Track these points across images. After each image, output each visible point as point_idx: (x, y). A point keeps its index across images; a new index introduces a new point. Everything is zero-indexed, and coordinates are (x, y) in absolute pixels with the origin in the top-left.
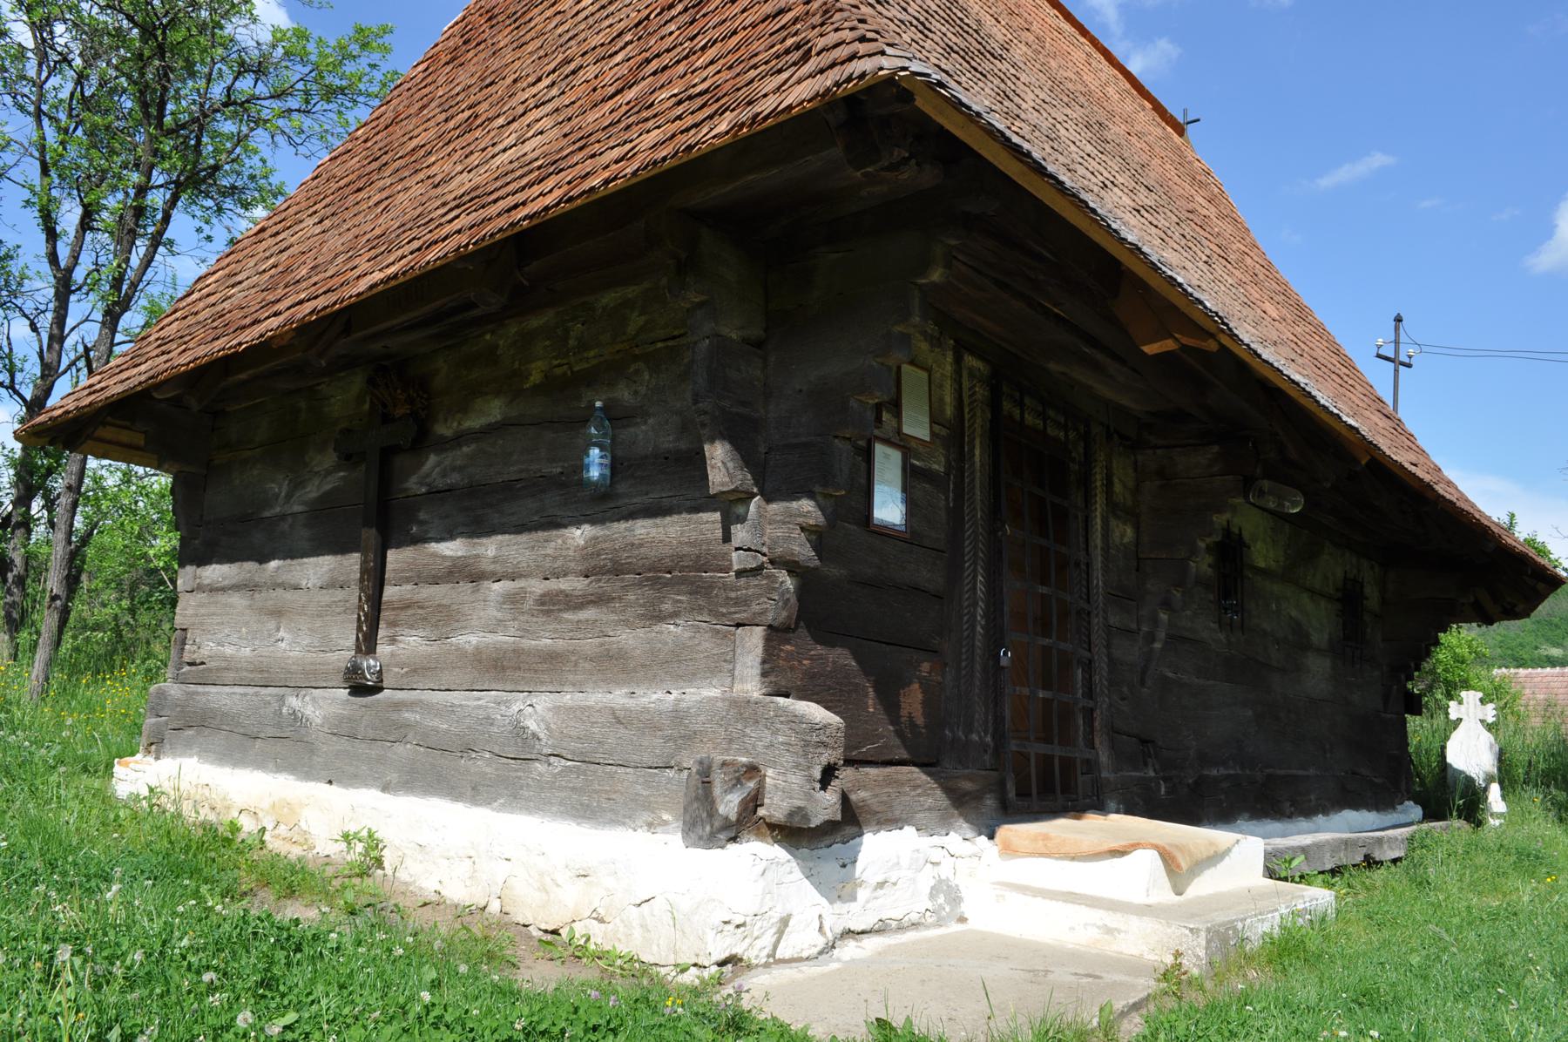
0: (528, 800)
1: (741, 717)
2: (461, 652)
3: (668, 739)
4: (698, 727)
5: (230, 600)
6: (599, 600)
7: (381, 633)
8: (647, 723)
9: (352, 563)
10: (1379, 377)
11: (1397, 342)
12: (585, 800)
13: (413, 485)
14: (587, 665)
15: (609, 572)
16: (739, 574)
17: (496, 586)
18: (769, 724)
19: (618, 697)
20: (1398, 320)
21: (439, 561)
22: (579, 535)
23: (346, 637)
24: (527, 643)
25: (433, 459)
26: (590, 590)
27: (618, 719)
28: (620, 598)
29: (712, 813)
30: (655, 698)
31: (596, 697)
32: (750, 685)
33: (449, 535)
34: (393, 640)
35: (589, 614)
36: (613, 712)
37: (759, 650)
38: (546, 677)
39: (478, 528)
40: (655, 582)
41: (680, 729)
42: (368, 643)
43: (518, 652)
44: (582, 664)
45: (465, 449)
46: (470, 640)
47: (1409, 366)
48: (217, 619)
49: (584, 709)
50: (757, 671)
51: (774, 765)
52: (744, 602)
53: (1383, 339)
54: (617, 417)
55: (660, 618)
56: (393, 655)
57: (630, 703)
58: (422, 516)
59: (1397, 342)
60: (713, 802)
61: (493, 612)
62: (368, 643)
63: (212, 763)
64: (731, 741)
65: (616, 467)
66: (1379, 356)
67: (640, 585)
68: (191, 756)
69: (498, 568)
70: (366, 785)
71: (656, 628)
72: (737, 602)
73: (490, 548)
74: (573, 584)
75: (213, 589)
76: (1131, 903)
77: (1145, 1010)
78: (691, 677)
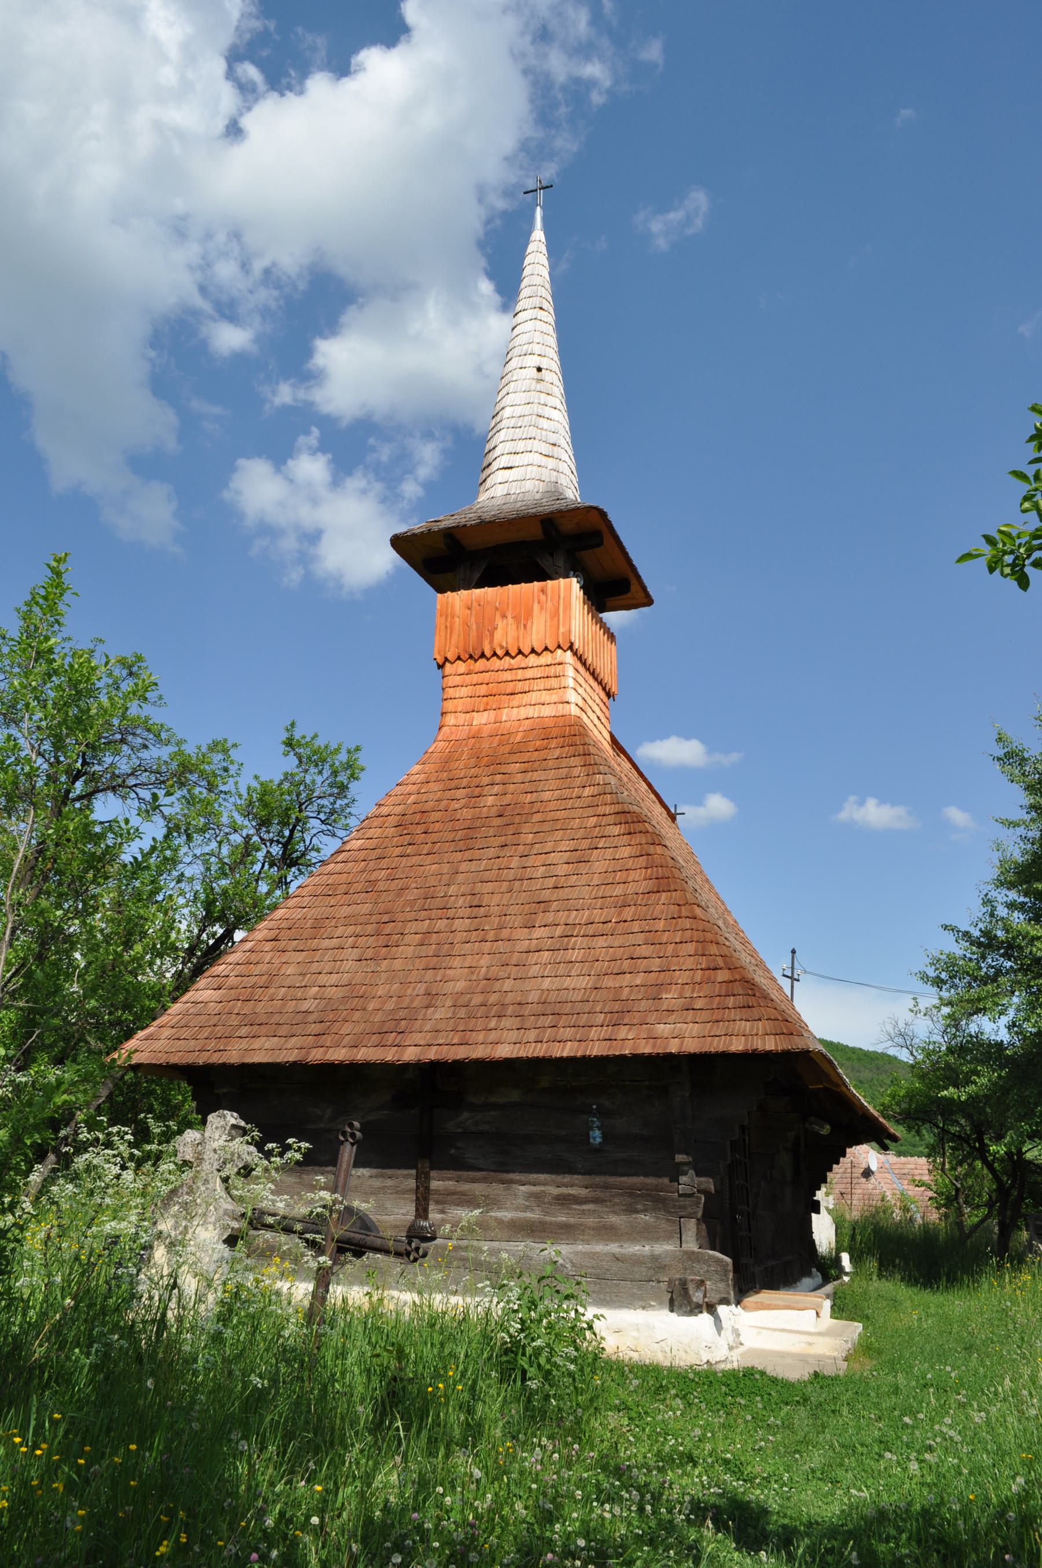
1: (689, 1259)
3: (649, 1268)
4: (667, 1263)
6: (596, 1201)
7: (431, 1207)
8: (637, 1261)
10: (785, 984)
11: (793, 968)
12: (602, 1297)
14: (591, 1232)
15: (601, 1187)
16: (680, 1195)
17: (522, 1188)
18: (706, 1262)
19: (614, 1248)
20: (793, 952)
24: (548, 1219)
25: (465, 1115)
26: (590, 1195)
27: (617, 1258)
28: (610, 1201)
29: (690, 1302)
30: (635, 1249)
31: (599, 1248)
32: (691, 1245)
36: (614, 1255)
37: (695, 1229)
40: (631, 1195)
41: (657, 1264)
42: (422, 1212)
44: (587, 1231)
45: (492, 1113)
46: (506, 1215)
47: (798, 980)
49: (594, 1253)
50: (694, 1239)
51: (710, 1280)
52: (684, 1207)
53: (786, 964)
54: (603, 1114)
55: (637, 1212)
57: (623, 1251)
59: (793, 968)
60: (690, 1297)
61: (522, 1202)
64: (686, 1269)
65: (604, 1136)
66: (784, 975)
67: (622, 1195)
71: (634, 1216)
72: (680, 1207)
77: (288, 1285)
78: (657, 1239)
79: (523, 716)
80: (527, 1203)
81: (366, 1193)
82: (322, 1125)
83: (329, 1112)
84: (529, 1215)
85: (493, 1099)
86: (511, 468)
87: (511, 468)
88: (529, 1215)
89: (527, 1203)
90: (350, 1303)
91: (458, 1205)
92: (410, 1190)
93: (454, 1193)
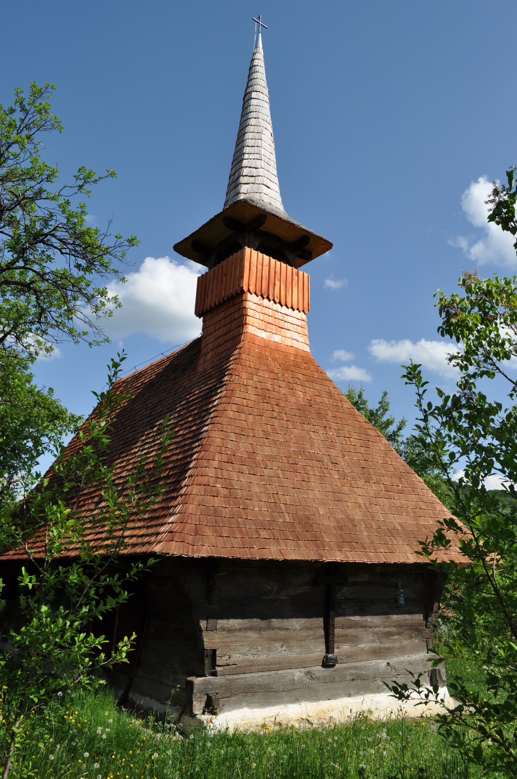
0: (255, 702)
2: (362, 649)
5: (246, 635)
6: (399, 634)
9: (320, 621)
13: (339, 596)
21: (350, 621)
22: (395, 617)
23: (323, 648)
24: (382, 646)
25: (345, 589)
33: (355, 615)
34: (338, 648)
35: (396, 637)
38: (388, 654)
39: (363, 613)
40: (410, 629)
42: (329, 649)
43: (380, 648)
48: (238, 644)
55: (412, 638)
56: (339, 652)
58: (343, 606)
62: (329, 649)
63: (258, 707)
65: (406, 600)
68: (243, 707)
69: (371, 624)
70: (342, 697)
73: (369, 619)
74: (393, 629)
75: (230, 631)
76: (335, 699)
79: (289, 345)
80: (373, 638)
81: (299, 641)
82: (272, 597)
83: (276, 588)
84: (374, 644)
85: (357, 580)
86: (269, 188)
87: (269, 188)
88: (374, 644)
89: (373, 638)
90: (93, 697)
91: (344, 643)
92: (322, 636)
93: (342, 636)
